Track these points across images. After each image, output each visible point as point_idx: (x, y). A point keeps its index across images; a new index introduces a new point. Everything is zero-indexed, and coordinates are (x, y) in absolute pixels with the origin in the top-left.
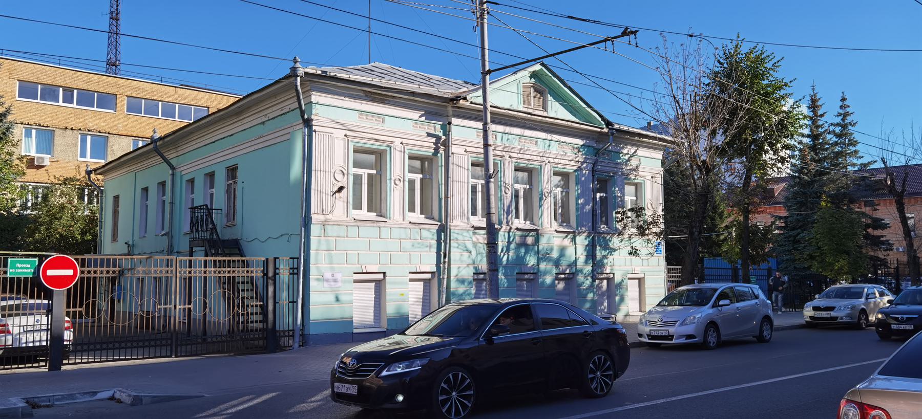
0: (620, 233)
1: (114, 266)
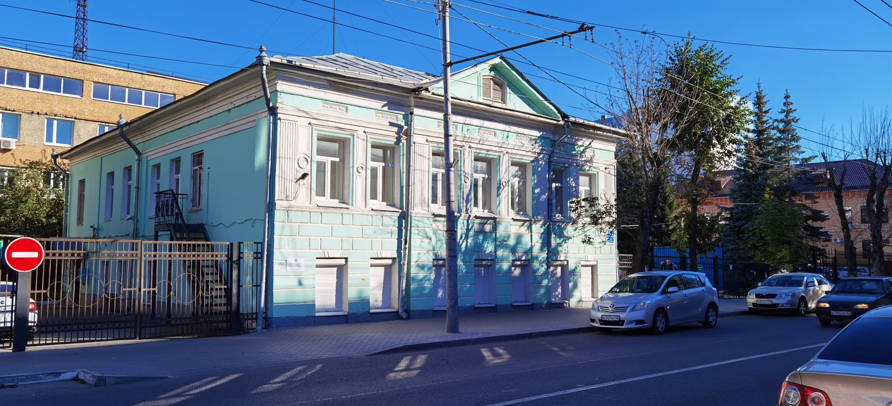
0: (574, 222)
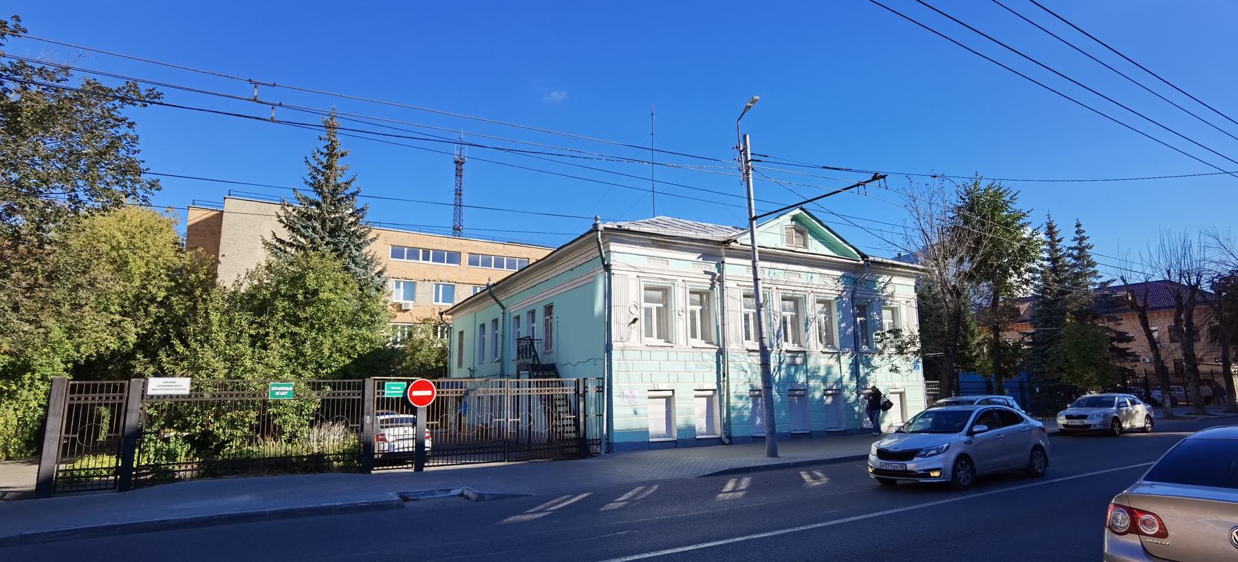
0: (881, 353)
1: (461, 388)
